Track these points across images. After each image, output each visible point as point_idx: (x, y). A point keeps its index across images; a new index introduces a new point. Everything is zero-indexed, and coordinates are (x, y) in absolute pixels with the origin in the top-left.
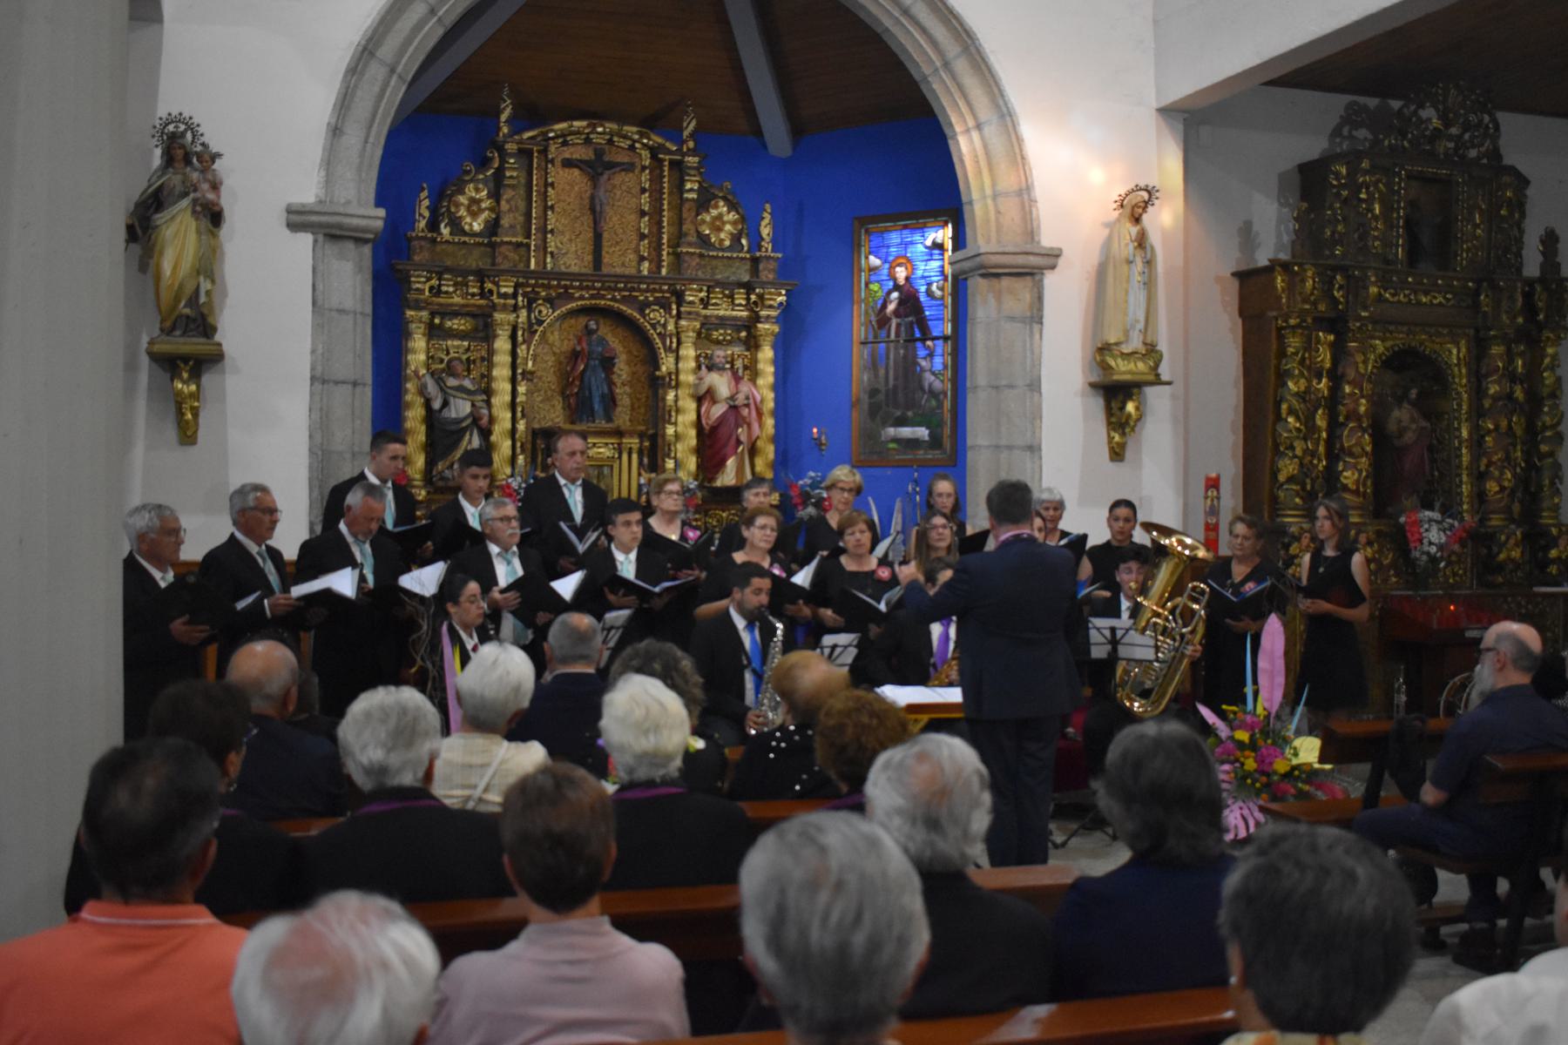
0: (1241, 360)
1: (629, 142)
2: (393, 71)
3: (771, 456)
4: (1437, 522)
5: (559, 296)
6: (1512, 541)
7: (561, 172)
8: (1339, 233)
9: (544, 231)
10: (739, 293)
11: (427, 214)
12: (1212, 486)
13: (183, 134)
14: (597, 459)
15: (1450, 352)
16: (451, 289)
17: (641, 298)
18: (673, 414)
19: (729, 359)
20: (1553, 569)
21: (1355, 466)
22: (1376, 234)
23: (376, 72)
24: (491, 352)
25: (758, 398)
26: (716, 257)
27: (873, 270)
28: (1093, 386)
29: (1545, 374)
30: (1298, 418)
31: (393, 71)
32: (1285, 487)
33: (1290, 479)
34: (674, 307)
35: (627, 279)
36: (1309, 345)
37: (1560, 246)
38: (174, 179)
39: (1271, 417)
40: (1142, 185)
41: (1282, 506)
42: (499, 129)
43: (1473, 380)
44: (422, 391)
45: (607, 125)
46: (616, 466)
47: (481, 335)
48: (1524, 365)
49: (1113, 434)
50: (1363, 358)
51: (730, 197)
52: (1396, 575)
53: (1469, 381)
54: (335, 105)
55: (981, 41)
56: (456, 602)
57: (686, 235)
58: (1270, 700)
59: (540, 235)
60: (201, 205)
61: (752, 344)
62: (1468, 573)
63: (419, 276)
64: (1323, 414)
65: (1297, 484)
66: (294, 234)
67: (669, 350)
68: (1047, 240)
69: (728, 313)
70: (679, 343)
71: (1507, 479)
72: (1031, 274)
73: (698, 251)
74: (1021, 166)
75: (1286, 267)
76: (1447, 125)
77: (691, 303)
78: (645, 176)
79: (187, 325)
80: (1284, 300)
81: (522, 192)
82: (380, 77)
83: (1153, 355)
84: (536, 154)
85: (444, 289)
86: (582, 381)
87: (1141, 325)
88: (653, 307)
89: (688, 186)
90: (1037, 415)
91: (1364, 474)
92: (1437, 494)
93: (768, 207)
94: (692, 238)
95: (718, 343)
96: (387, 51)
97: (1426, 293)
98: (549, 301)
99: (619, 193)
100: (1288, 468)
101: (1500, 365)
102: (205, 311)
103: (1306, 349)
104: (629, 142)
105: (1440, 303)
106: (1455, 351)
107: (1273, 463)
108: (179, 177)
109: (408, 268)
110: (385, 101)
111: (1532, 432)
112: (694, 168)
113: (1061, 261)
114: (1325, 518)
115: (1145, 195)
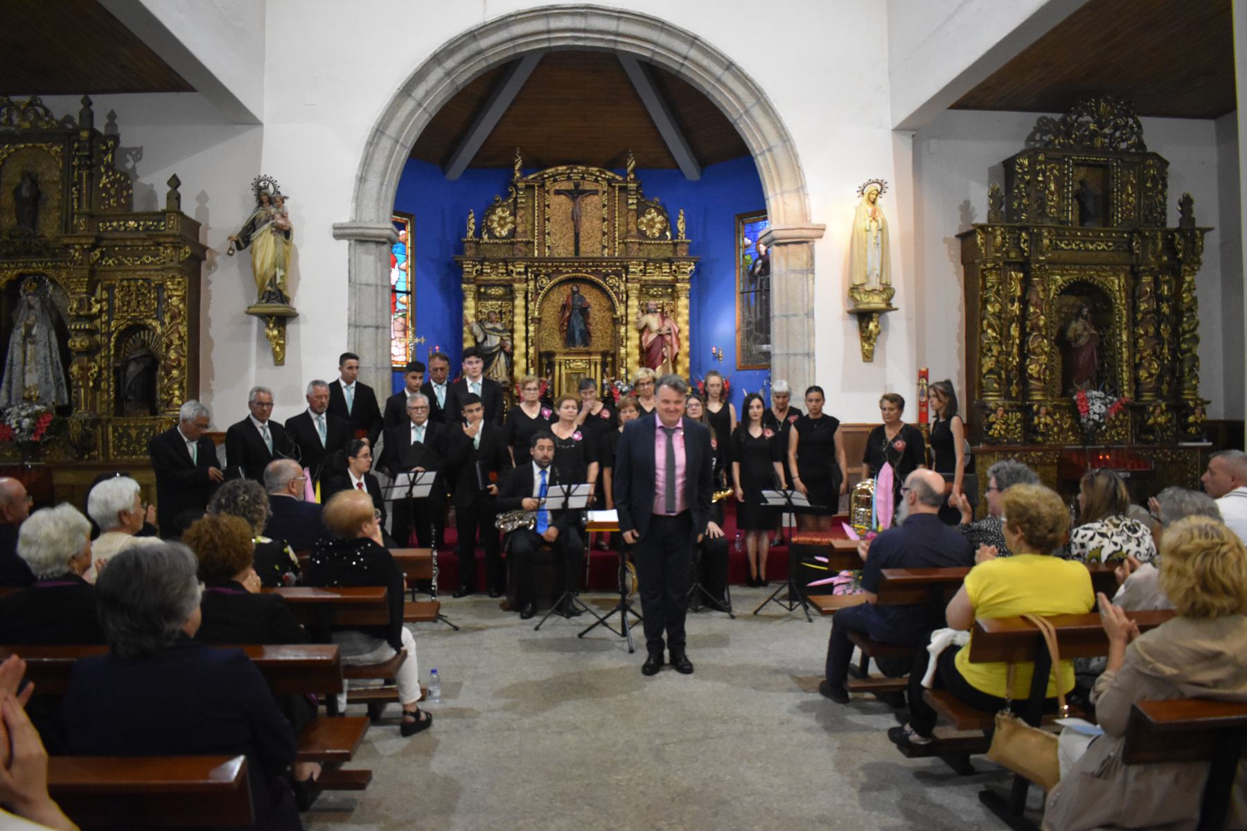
0: (963, 293)
2: (397, 142)
4: (1100, 398)
5: (553, 271)
6: (1158, 411)
8: (1024, 205)
9: (543, 233)
11: (473, 227)
12: (923, 377)
13: (266, 187)
14: (576, 369)
15: (1113, 282)
16: (489, 271)
18: (624, 341)
20: (1193, 430)
23: (386, 143)
24: (514, 307)
26: (651, 244)
27: (747, 247)
28: (850, 312)
29: (1184, 295)
30: (994, 330)
31: (397, 142)
33: (990, 371)
34: (624, 275)
35: (593, 259)
36: (1004, 281)
37: (1194, 206)
38: (262, 214)
40: (874, 179)
42: (514, 174)
43: (1129, 300)
44: (471, 332)
47: (508, 297)
48: (1169, 289)
49: (864, 344)
50: (1042, 288)
53: (1127, 302)
54: (360, 164)
56: (355, 457)
58: (885, 522)
59: (541, 237)
60: (275, 227)
61: (674, 296)
62: (1129, 433)
67: (621, 301)
68: (816, 220)
69: (659, 278)
70: (628, 297)
72: (807, 242)
75: (982, 228)
76: (1102, 128)
77: (633, 272)
78: (605, 197)
79: (269, 297)
80: (983, 251)
81: (530, 211)
82: (389, 146)
85: (485, 271)
87: (878, 272)
89: (630, 201)
90: (811, 334)
91: (1044, 366)
92: (1105, 379)
93: (682, 211)
94: (634, 233)
95: (654, 296)
97: (1092, 243)
98: (549, 276)
99: (589, 208)
100: (988, 363)
101: (1148, 290)
102: (281, 288)
103: (1000, 284)
104: (594, 177)
106: (1117, 281)
107: (980, 360)
108: (264, 212)
110: (393, 158)
111: (1175, 334)
112: (633, 190)
113: (826, 233)
114: (934, 396)
115: (879, 187)
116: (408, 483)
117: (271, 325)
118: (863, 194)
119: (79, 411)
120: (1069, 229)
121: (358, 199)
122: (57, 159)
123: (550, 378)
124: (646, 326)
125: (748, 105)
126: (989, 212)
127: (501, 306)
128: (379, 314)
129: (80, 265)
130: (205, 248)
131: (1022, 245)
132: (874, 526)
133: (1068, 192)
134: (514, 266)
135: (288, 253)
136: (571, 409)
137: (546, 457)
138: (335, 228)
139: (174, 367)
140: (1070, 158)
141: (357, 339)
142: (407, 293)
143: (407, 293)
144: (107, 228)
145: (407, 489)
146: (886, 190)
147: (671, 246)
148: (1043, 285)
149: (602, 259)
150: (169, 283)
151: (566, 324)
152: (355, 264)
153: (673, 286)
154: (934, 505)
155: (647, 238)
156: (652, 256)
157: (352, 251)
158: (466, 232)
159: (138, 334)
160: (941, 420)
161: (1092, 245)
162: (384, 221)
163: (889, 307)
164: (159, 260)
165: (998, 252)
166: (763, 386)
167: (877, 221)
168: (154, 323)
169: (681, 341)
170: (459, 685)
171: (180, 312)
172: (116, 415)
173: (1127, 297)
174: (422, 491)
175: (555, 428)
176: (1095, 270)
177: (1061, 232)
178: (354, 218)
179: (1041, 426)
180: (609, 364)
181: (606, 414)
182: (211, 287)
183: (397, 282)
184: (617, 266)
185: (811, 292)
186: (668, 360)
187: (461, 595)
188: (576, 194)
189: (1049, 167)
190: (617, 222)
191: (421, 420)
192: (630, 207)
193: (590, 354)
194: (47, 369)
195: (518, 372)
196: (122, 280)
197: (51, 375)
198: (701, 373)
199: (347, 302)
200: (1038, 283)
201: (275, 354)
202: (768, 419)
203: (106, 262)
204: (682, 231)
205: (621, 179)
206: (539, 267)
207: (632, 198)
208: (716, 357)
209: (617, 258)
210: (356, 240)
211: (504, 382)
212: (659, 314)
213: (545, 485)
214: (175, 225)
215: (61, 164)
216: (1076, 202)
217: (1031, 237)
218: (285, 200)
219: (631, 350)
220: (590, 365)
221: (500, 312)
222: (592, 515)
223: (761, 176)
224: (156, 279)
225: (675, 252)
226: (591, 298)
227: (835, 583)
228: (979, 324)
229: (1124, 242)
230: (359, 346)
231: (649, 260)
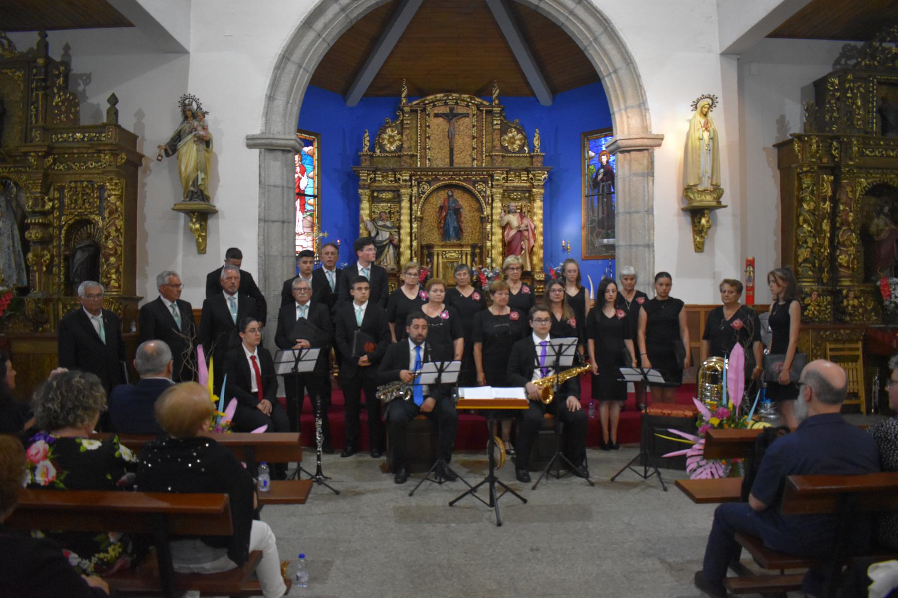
0: (780, 193)
1: (466, 103)
2: (300, 67)
3: (541, 255)
5: (433, 180)
8: (835, 117)
9: (424, 148)
11: (368, 144)
12: (750, 265)
13: (190, 104)
16: (380, 179)
17: (474, 179)
18: (490, 235)
21: (846, 252)
22: (859, 117)
23: (291, 68)
24: (400, 208)
25: (533, 227)
26: (512, 157)
27: (591, 158)
28: (684, 210)
30: (809, 225)
31: (300, 67)
32: (802, 265)
33: (805, 260)
34: (490, 182)
35: (465, 169)
36: (817, 183)
39: (795, 225)
40: (706, 94)
41: (801, 276)
42: (401, 101)
44: (366, 229)
45: (453, 95)
49: (696, 237)
50: (851, 189)
51: (518, 127)
52: (876, 315)
55: (614, 24)
56: (244, 333)
57: (495, 146)
58: (736, 398)
60: (197, 137)
61: (531, 199)
63: (364, 173)
64: (827, 222)
65: (809, 263)
66: (250, 150)
67: (487, 204)
68: (655, 130)
69: (519, 184)
70: (493, 200)
74: (639, 91)
75: (799, 137)
77: (498, 180)
81: (414, 130)
82: (293, 71)
83: (718, 191)
84: (419, 112)
85: (377, 179)
87: (709, 174)
89: (495, 122)
90: (651, 228)
91: (852, 256)
93: (537, 130)
95: (514, 200)
96: (297, 56)
97: (893, 151)
98: (429, 183)
99: (462, 128)
100: (804, 253)
102: (202, 188)
103: (814, 185)
104: (466, 103)
107: (796, 252)
109: (358, 169)
113: (664, 142)
115: (710, 101)
116: (294, 359)
117: (194, 220)
118: (696, 108)
119: (35, 291)
121: (268, 114)
122: (19, 82)
123: (430, 266)
124: (508, 224)
125: (597, 34)
126: (805, 124)
127: (390, 207)
128: (285, 211)
129: (36, 169)
130: (141, 157)
131: (833, 152)
132: (724, 402)
133: (872, 107)
134: (401, 175)
135: (208, 159)
136: (438, 293)
137: (420, 335)
138: (248, 139)
139: (112, 255)
140: (874, 77)
142: (314, 196)
143: (314, 196)
144: (59, 139)
145: (293, 365)
147: (529, 159)
148: (851, 187)
150: (108, 184)
151: (442, 222)
153: (530, 191)
154: (834, 402)
155: (509, 152)
156: (513, 167)
157: (262, 157)
158: (362, 147)
159: (85, 228)
160: (781, 303)
161: (893, 152)
163: (720, 206)
164: (101, 165)
165: (814, 158)
166: (605, 273)
167: (709, 131)
168: (97, 218)
169: (537, 236)
170: (329, 564)
171: (117, 209)
172: (66, 294)
174: (307, 366)
175: (425, 308)
178: (264, 131)
179: (850, 307)
180: (478, 255)
181: (477, 297)
182: (146, 189)
183: (306, 188)
184: (484, 175)
185: (650, 192)
186: (525, 252)
187: (349, 455)
188: (451, 116)
189: (856, 85)
190: (484, 139)
191: (305, 299)
192: (495, 127)
193: (461, 246)
194: (10, 256)
195: (403, 260)
196: (70, 182)
197: (13, 261)
198: (552, 262)
200: (847, 184)
201: (198, 245)
202: (619, 302)
203: (58, 167)
204: (537, 146)
205: (488, 104)
206: (420, 176)
207: (497, 120)
208: (565, 249)
209: (485, 168)
210: (266, 149)
211: (393, 269)
212: (518, 214)
213: (420, 362)
214: (114, 136)
215: (22, 87)
216: (878, 116)
217: (841, 145)
218: (206, 115)
219: (496, 241)
220: (462, 256)
221: (390, 212)
222: (463, 392)
223: (607, 95)
224: (98, 182)
225: (532, 163)
226: (463, 201)
227: (689, 455)
230: (268, 238)
231: (511, 170)
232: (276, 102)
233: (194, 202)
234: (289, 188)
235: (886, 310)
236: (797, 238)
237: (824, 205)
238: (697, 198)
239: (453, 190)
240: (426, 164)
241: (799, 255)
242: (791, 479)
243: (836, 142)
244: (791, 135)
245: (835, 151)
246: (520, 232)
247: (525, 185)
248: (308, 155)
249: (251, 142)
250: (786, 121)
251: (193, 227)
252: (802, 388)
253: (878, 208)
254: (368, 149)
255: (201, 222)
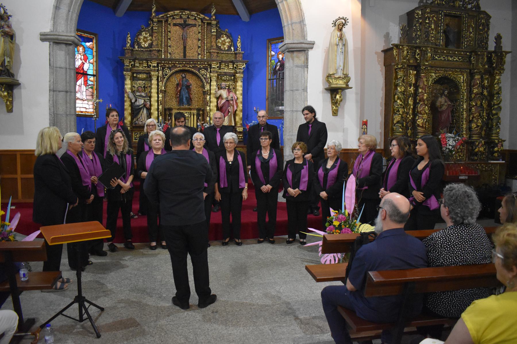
1: (194, 17)
4: (452, 138)
5: (172, 66)
6: (480, 145)
7: (173, 27)
8: (418, 35)
9: (167, 46)
10: (230, 65)
12: (364, 124)
15: (460, 78)
16: (138, 65)
18: (209, 103)
19: (228, 86)
25: (236, 98)
26: (223, 53)
27: (272, 56)
28: (327, 89)
29: (495, 86)
30: (401, 101)
33: (398, 122)
34: (209, 69)
35: (193, 60)
36: (406, 75)
40: (341, 17)
42: (152, 14)
44: (129, 97)
45: (186, 12)
46: (190, 120)
48: (488, 82)
49: (333, 106)
51: (227, 34)
53: (467, 88)
58: (350, 209)
61: (235, 81)
63: (127, 61)
65: (400, 124)
67: (207, 83)
68: (310, 38)
70: (211, 81)
71: (479, 123)
73: (216, 51)
75: (397, 46)
77: (214, 68)
78: (200, 28)
84: (163, 22)
85: (136, 65)
86: (180, 93)
87: (342, 67)
88: (202, 69)
89: (213, 31)
91: (425, 120)
93: (239, 37)
94: (215, 47)
95: (224, 81)
97: (451, 57)
98: (170, 68)
99: (191, 34)
101: (478, 82)
102: (8, 68)
103: (405, 76)
104: (194, 17)
105: (457, 60)
106: (462, 78)
107: (393, 116)
109: (123, 58)
111: (490, 106)
113: (315, 46)
115: (344, 22)
117: (3, 90)
120: (440, 49)
121: (55, 18)
123: (170, 122)
126: (400, 38)
127: (145, 84)
133: (441, 30)
134: (151, 63)
135: (12, 48)
141: (55, 98)
142: (93, 75)
143: (93, 75)
146: (348, 23)
149: (198, 60)
152: (53, 56)
153: (234, 76)
154: (400, 222)
155: (221, 50)
156: (224, 60)
158: (126, 44)
162: (70, 32)
163: (348, 87)
165: (405, 60)
173: (467, 86)
176: (452, 71)
177: (436, 50)
183: (88, 70)
184: (205, 65)
185: (306, 78)
188: (184, 26)
192: (212, 34)
193: (190, 109)
198: (248, 120)
199: (48, 77)
201: (7, 106)
204: (239, 47)
206: (163, 63)
207: (214, 29)
210: (53, 42)
216: (444, 35)
218: (10, 17)
220: (191, 116)
221: (144, 87)
225: (236, 58)
226: (192, 81)
228: (392, 97)
229: (467, 57)
231: (222, 62)
232: (61, 11)
233: (3, 77)
234: (70, 69)
235: (444, 153)
236: (393, 108)
237: (410, 89)
238: (334, 82)
239: (185, 74)
240: (168, 56)
241: (394, 119)
242: (371, 273)
243: (419, 50)
244: (392, 45)
245: (417, 56)
246: (228, 101)
247: (231, 71)
248: (89, 48)
249: (43, 37)
250: (390, 36)
251: (3, 95)
252: (381, 210)
253: (442, 91)
254: (130, 45)
255: (8, 91)
